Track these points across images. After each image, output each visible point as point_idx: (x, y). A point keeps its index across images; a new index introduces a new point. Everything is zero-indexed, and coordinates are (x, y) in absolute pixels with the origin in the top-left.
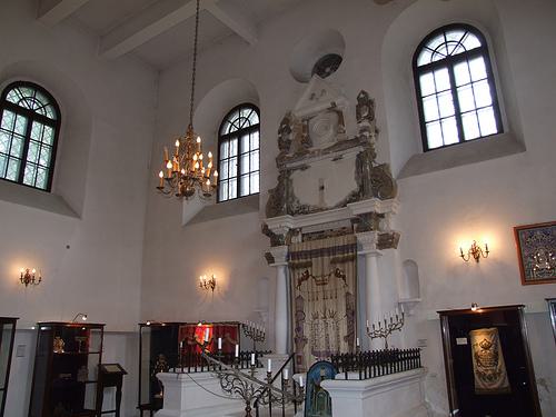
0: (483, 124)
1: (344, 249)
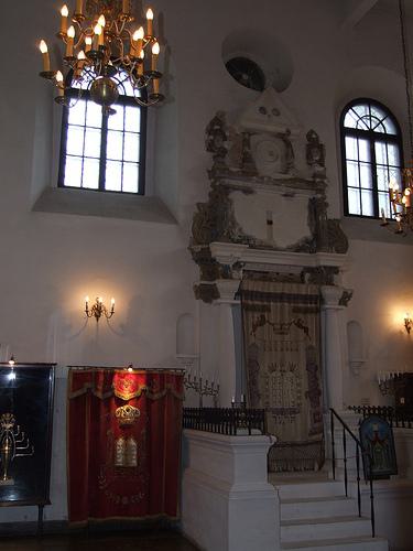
0: (124, 179)
1: (306, 298)
